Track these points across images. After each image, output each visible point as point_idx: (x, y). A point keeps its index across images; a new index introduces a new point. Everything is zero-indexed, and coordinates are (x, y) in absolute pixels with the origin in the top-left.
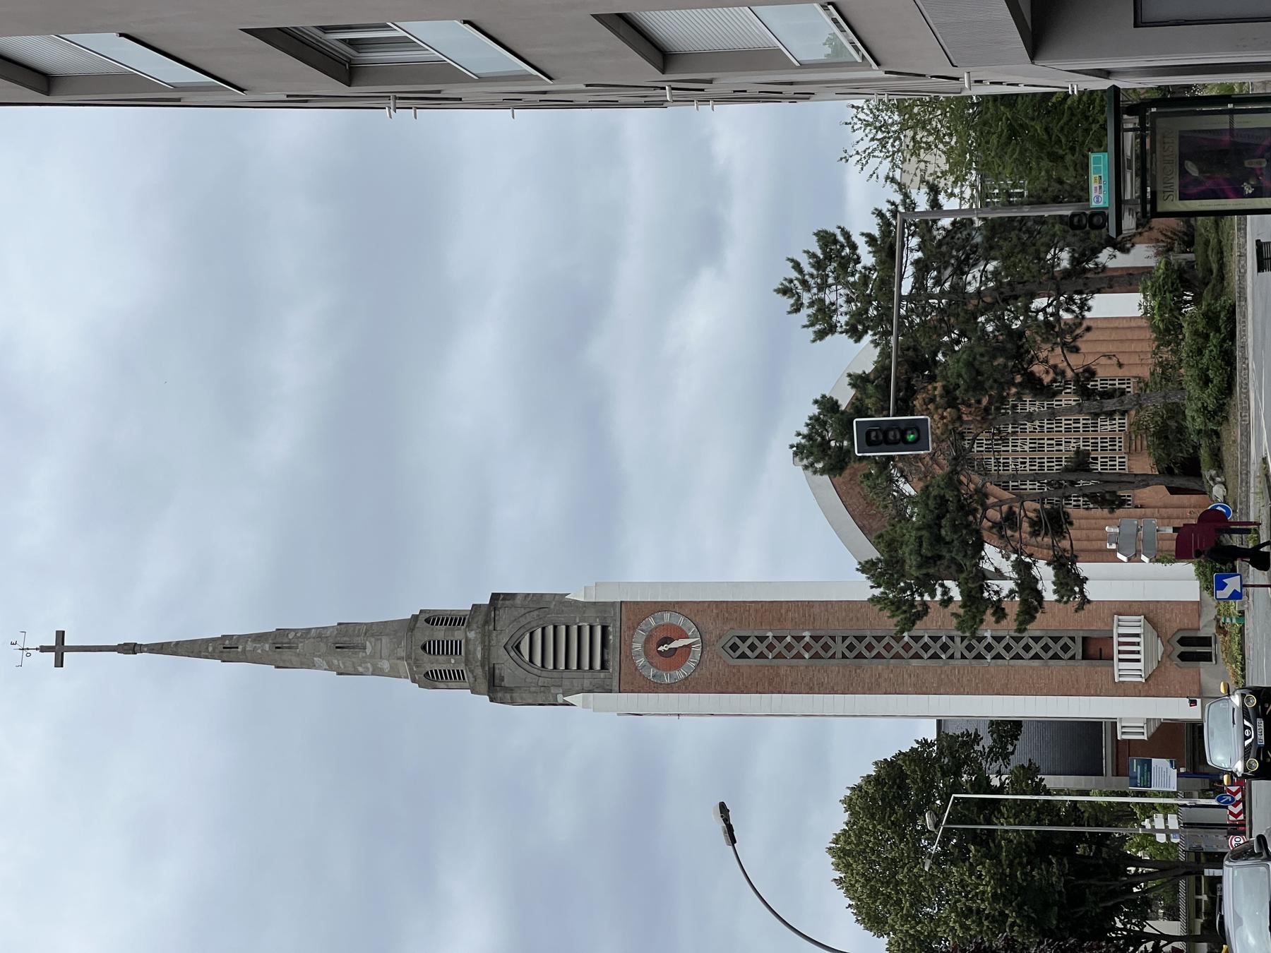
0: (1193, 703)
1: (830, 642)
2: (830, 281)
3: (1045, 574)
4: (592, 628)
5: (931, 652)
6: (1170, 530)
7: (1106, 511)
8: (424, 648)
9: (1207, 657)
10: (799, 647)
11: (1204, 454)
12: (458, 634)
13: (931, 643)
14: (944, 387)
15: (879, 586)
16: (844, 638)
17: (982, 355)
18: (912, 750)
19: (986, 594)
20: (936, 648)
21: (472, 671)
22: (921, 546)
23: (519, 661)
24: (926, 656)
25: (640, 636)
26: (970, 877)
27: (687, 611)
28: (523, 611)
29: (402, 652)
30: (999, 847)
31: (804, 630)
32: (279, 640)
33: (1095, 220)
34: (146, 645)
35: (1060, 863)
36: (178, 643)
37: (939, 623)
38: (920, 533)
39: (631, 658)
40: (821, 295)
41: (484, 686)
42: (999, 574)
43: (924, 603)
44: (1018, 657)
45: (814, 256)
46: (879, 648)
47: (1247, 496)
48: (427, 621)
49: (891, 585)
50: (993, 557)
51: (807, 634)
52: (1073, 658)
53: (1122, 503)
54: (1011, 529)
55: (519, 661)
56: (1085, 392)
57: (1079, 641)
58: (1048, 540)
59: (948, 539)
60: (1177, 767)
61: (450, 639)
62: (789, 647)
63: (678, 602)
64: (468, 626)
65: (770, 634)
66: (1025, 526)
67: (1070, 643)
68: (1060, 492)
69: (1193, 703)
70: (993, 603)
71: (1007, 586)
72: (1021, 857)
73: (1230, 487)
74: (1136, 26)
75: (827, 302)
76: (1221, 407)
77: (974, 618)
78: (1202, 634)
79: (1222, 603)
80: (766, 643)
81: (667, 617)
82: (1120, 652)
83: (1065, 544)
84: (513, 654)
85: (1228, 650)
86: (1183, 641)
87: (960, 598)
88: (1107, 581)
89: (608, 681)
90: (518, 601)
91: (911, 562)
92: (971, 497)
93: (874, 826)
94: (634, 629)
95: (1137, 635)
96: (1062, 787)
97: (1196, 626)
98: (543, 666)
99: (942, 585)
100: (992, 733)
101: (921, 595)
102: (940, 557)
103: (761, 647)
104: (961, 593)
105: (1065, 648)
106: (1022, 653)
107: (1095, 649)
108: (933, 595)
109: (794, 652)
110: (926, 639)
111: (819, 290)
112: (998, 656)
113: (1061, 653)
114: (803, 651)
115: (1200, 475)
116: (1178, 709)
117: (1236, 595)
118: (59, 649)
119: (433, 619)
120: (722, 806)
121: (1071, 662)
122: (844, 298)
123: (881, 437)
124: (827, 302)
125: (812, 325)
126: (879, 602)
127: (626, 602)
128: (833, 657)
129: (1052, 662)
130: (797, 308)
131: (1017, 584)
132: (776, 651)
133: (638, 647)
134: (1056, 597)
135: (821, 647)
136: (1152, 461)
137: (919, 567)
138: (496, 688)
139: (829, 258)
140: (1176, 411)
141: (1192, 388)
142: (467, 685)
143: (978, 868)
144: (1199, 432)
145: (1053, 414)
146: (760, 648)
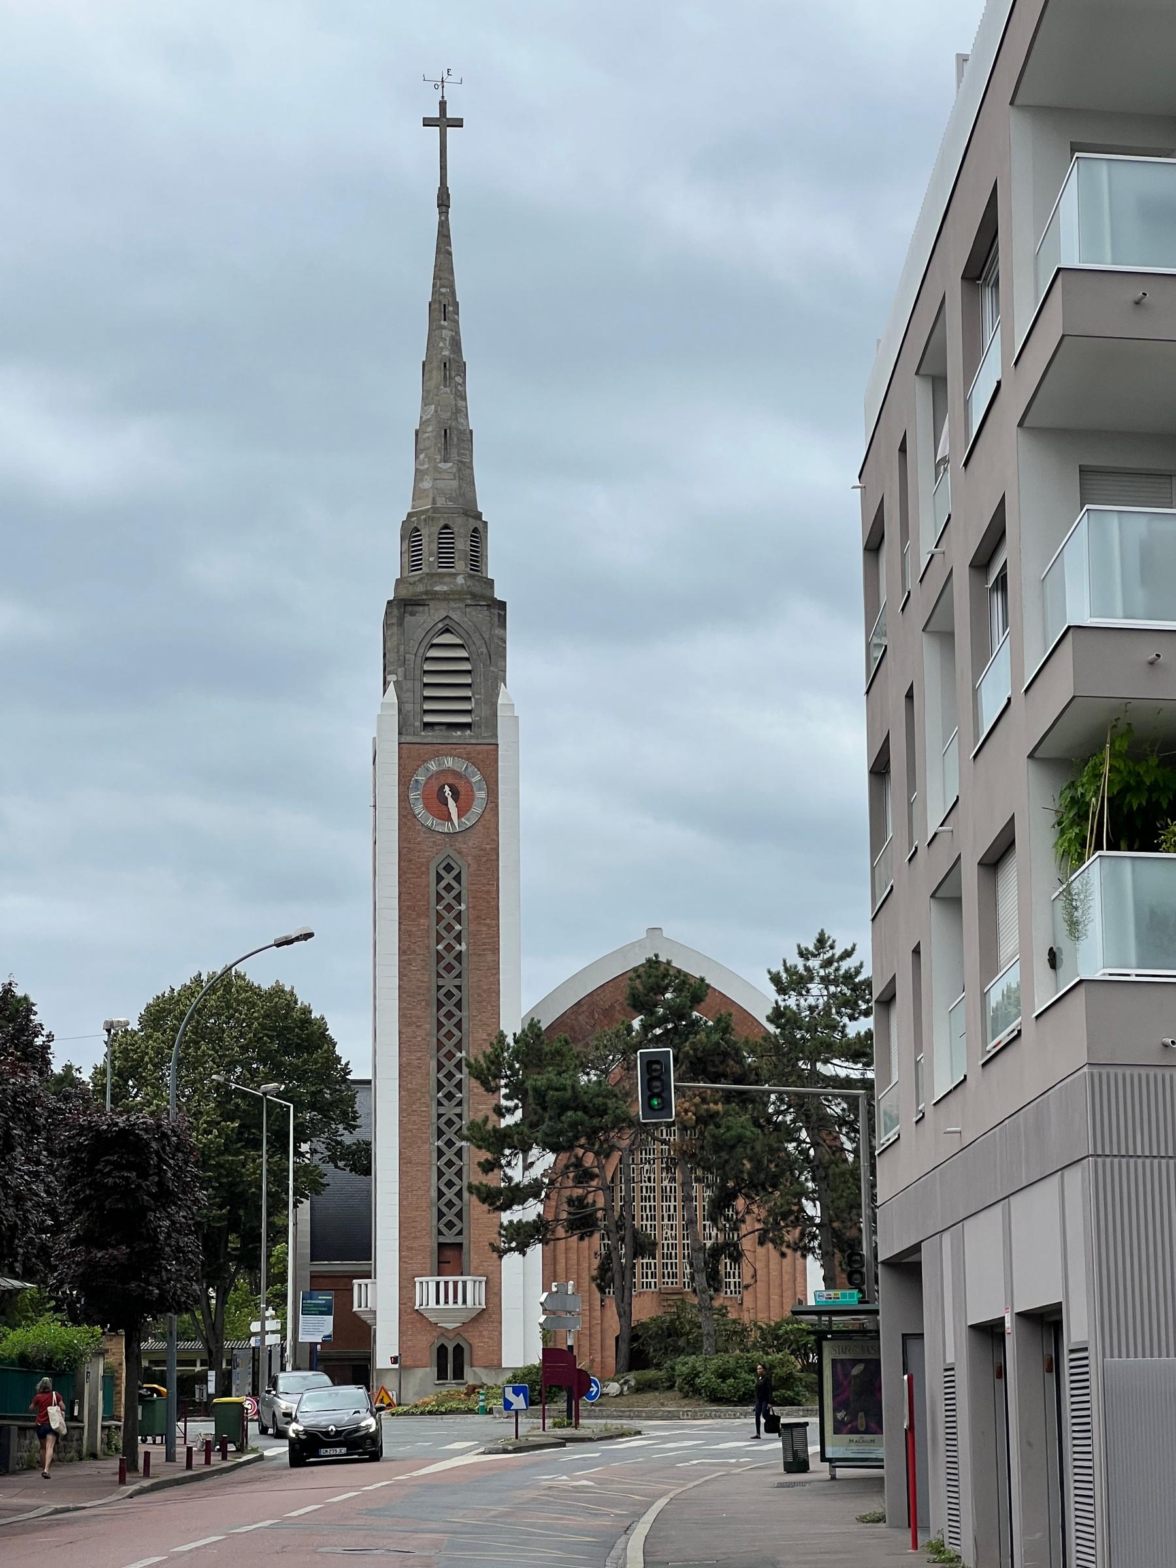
0: (395, 1360)
1: (455, 973)
2: (832, 989)
3: (530, 1211)
4: (469, 712)
5: (444, 1081)
6: (569, 1343)
7: (595, 1273)
8: (446, 527)
9: (442, 1375)
10: (449, 938)
11: (651, 1374)
12: (461, 566)
13: (455, 1081)
14: (718, 1113)
15: (516, 1042)
16: (459, 988)
17: (753, 1148)
18: (339, 1059)
19: (507, 1152)
20: (449, 1086)
21: (420, 580)
22: (557, 1090)
23: (432, 633)
24: (440, 1076)
25: (460, 765)
26: (206, 1122)
27: (487, 816)
28: (487, 636)
29: (441, 502)
30: (238, 1153)
31: (468, 945)
32: (454, 366)
33: (857, 1276)
34: (447, 219)
35: (220, 1218)
36: (450, 254)
37: (477, 1105)
38: (569, 1088)
39: (436, 755)
40: (817, 980)
41: (404, 593)
42: (528, 1166)
43: (498, 1088)
44: (440, 1174)
45: (858, 972)
46: (449, 1025)
47: (608, 1417)
48: (475, 530)
49: (516, 1055)
50: (544, 1161)
51: (463, 947)
52: (440, 1233)
53: (602, 1290)
54: (575, 1177)
55: (432, 633)
56: (716, 1252)
57: (458, 1240)
58: (564, 1215)
59: (563, 1118)
60: (323, 1343)
61: (456, 555)
62: (449, 928)
63: (497, 806)
64: (471, 576)
65: (463, 907)
66: (579, 1192)
67: (456, 1230)
68: (613, 1228)
69: (395, 1360)
70: (498, 1160)
71: (516, 1174)
72: (227, 1176)
73: (617, 1399)
74: (903, 1335)
75: (809, 986)
76: (697, 1391)
77: (483, 1140)
78: (467, 1370)
79: (500, 1391)
80: (454, 903)
81: (481, 795)
82: (446, 1283)
83: (561, 1232)
84: (440, 625)
85: (450, 1397)
86: (458, 1349)
87: (502, 1126)
88: (522, 1278)
89: (411, 730)
90: (497, 631)
91: (539, 1080)
92: (606, 1140)
93: (257, 1019)
94: (468, 759)
95: (464, 1302)
96: (299, 1218)
97: (475, 1363)
98: (427, 659)
99: (516, 1107)
100: (358, 1144)
101: (506, 1086)
102: (545, 1109)
103: (449, 898)
104: (508, 1126)
105: (450, 1225)
106: (445, 1179)
107: (449, 1257)
108: (507, 1097)
109: (444, 933)
110: (459, 1076)
111: (822, 978)
112: (440, 1154)
113: (445, 1220)
114: (445, 943)
115: (630, 1370)
116: (386, 1347)
117: (508, 1405)
118: (443, 122)
119: (478, 535)
120: (311, 935)
121: (435, 1231)
122: (813, 1003)
123: (655, 1074)
124: (809, 986)
125: (787, 970)
126: (499, 1042)
127: (497, 750)
128: (439, 975)
129: (435, 1210)
130: (804, 954)
131: (518, 1184)
132: (444, 913)
133: (449, 763)
134: (506, 1223)
135: (449, 963)
136: (645, 1318)
137: (535, 1089)
138: (402, 607)
139: (855, 988)
140: (695, 1347)
141: (716, 1362)
142: (406, 574)
143: (215, 1132)
144: (673, 1369)
145: (691, 1223)
146: (448, 900)
